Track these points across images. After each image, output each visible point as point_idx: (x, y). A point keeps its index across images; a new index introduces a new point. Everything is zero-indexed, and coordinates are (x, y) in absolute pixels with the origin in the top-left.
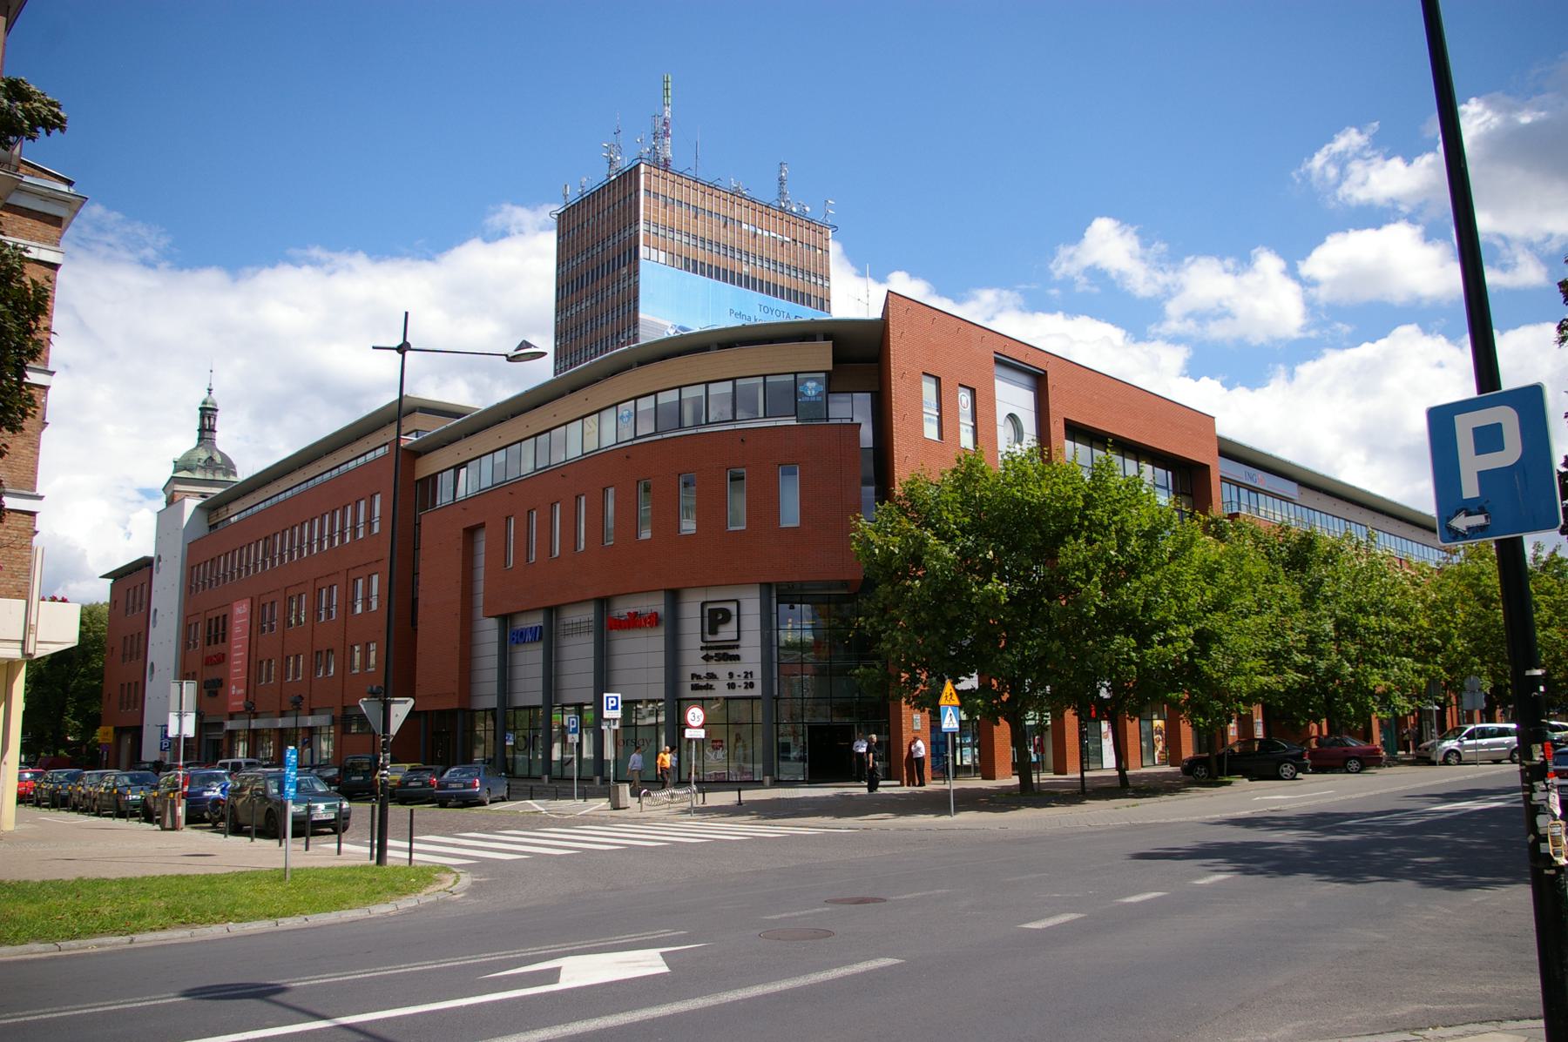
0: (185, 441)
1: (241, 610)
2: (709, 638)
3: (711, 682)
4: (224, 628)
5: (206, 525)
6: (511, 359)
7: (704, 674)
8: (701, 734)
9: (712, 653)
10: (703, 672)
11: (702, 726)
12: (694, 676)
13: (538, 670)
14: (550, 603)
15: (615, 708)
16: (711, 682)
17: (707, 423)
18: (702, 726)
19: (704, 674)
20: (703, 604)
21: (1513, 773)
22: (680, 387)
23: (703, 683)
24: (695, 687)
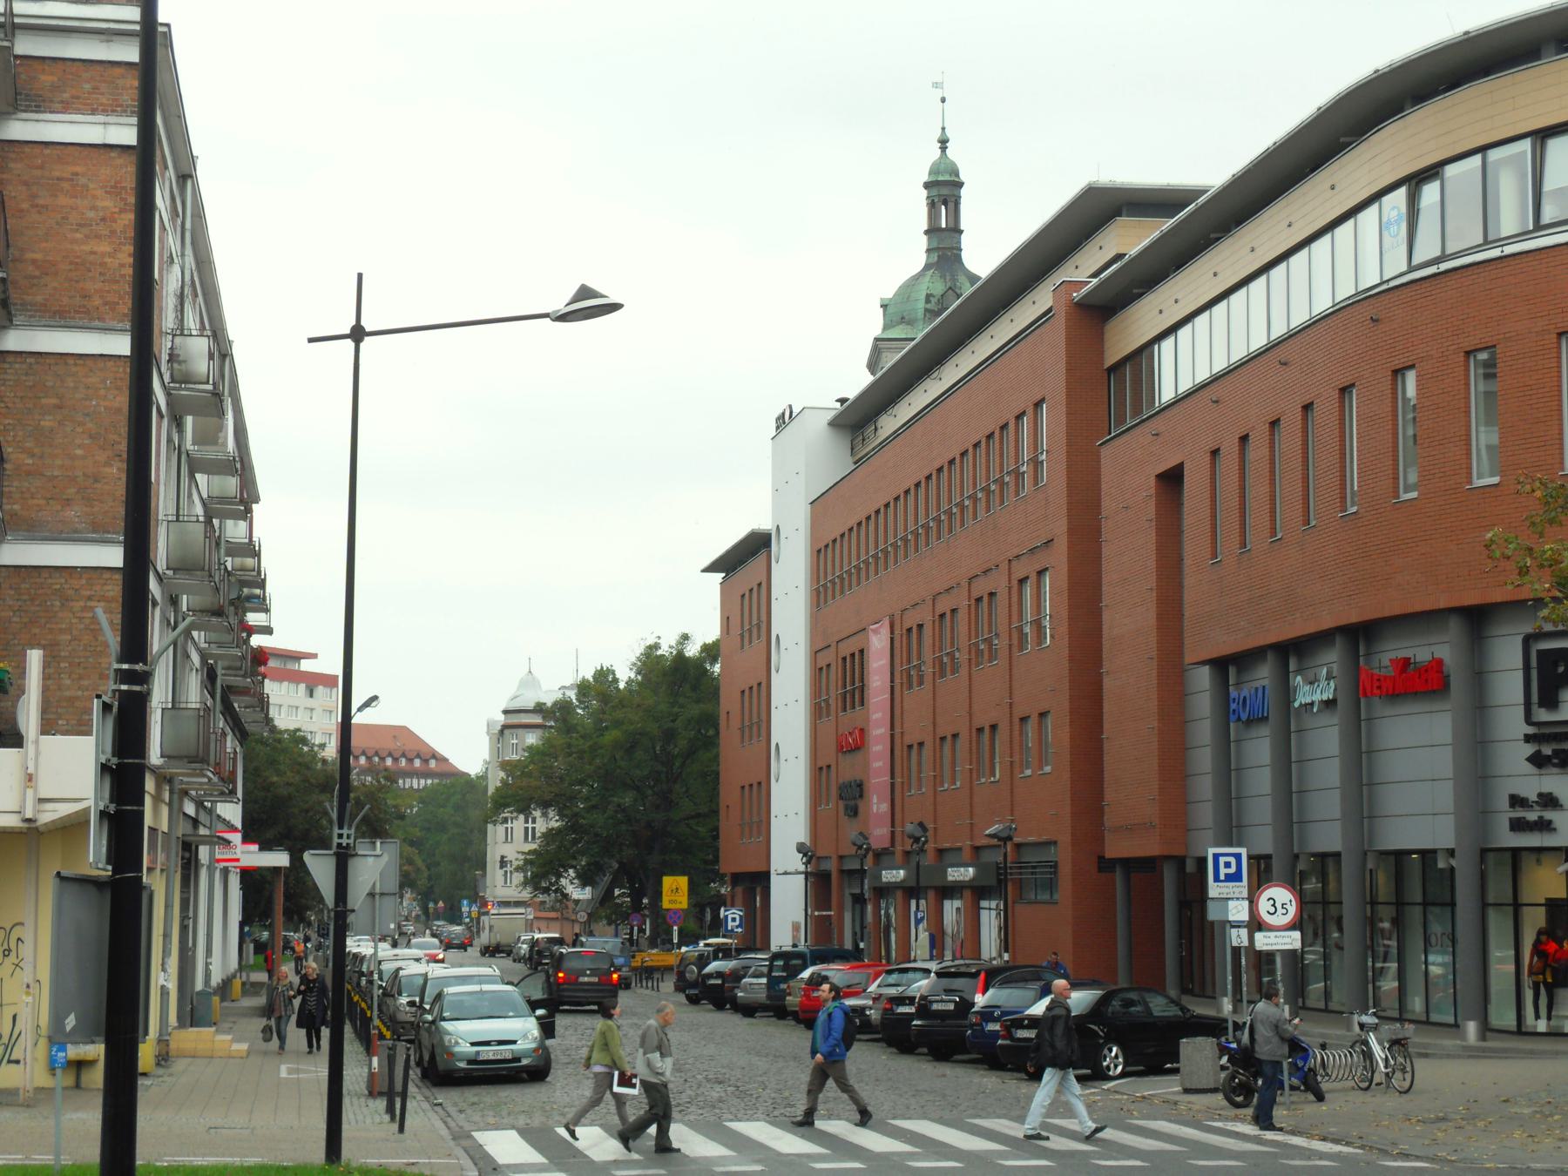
0: (913, 255)
1: (878, 642)
2: (1543, 715)
3: (1549, 815)
4: (862, 680)
5: (850, 460)
6: (563, 318)
7: (1533, 797)
8: (1293, 940)
9: (1547, 750)
10: (1530, 791)
11: (1291, 927)
12: (1517, 801)
13: (1443, 762)
14: (1471, 599)
15: (1236, 877)
16: (1549, 815)
17: (1539, 226)
18: (1291, 927)
19: (1533, 797)
20: (1528, 640)
21: (830, 1117)
22: (1483, 149)
23: (1532, 816)
24: (1518, 826)
